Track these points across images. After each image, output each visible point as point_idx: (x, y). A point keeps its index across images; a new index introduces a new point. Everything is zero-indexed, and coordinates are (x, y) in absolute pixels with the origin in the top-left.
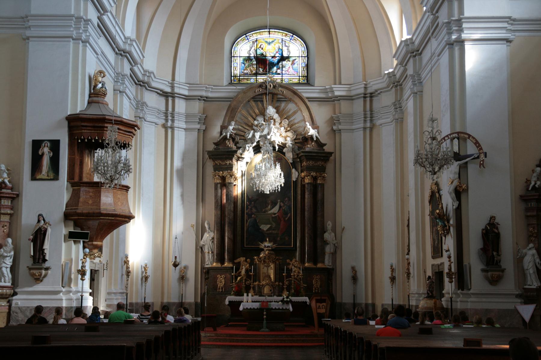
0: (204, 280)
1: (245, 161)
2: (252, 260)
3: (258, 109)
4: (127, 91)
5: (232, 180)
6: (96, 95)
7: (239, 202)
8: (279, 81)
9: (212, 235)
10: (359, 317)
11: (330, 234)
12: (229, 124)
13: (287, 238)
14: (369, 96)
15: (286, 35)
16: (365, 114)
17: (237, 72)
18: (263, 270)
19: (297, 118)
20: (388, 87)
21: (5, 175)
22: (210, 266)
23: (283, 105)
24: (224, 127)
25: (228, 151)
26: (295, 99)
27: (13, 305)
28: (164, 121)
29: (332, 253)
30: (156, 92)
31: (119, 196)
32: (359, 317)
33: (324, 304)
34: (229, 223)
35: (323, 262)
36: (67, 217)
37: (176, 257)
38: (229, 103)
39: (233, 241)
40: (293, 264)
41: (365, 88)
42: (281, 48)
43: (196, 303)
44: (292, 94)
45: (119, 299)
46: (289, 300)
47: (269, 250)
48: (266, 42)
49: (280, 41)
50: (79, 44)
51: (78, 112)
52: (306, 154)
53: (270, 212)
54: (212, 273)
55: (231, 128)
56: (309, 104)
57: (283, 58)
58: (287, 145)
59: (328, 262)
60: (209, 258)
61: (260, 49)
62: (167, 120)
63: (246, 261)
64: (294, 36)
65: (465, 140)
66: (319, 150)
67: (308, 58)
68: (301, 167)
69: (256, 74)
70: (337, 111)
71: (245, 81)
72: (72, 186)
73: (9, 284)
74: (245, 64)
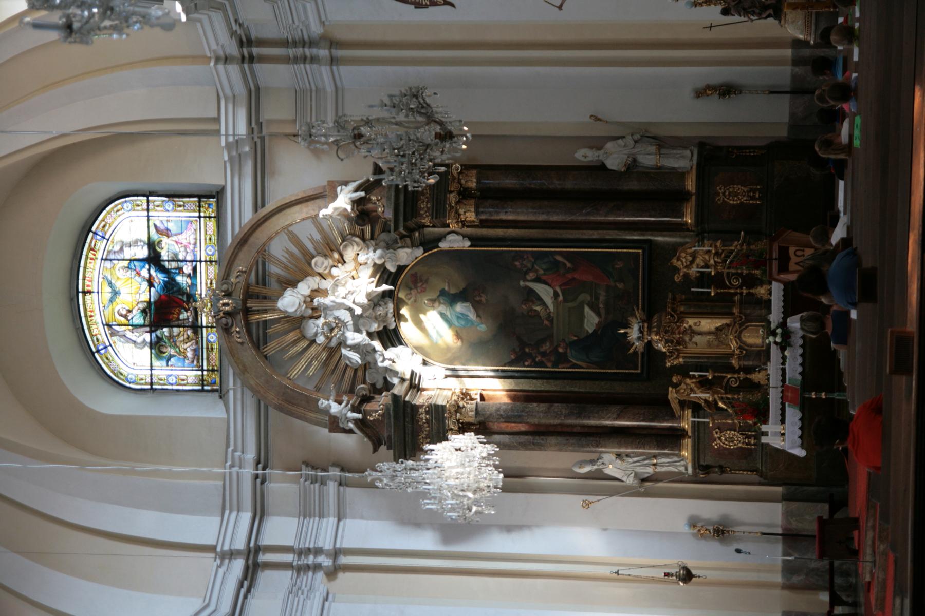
0: (725, 476)
1: (420, 369)
5: (471, 405)
7: (525, 385)
8: (213, 270)
10: (829, 330)
12: (326, 411)
13: (619, 265)
14: (249, 48)
15: (91, 249)
16: (295, 60)
17: (192, 375)
18: (700, 345)
23: (274, 269)
25: (396, 418)
28: (320, 575)
30: (245, 597)
32: (829, 330)
33: (792, 250)
34: (579, 415)
35: (681, 175)
38: (271, 409)
39: (625, 403)
40: (687, 267)
41: (227, 60)
42: (126, 263)
43: (786, 498)
44: (245, 248)
46: (779, 331)
47: (650, 328)
48: (111, 301)
49: (108, 264)
52: (401, 218)
54: (708, 460)
55: (335, 408)
56: (270, 207)
57: (154, 259)
58: (379, 262)
59: (683, 161)
61: (130, 316)
62: (317, 567)
63: (676, 386)
64: (93, 229)
69: (196, 328)
70: (289, 130)
71: (215, 355)
74: (171, 356)
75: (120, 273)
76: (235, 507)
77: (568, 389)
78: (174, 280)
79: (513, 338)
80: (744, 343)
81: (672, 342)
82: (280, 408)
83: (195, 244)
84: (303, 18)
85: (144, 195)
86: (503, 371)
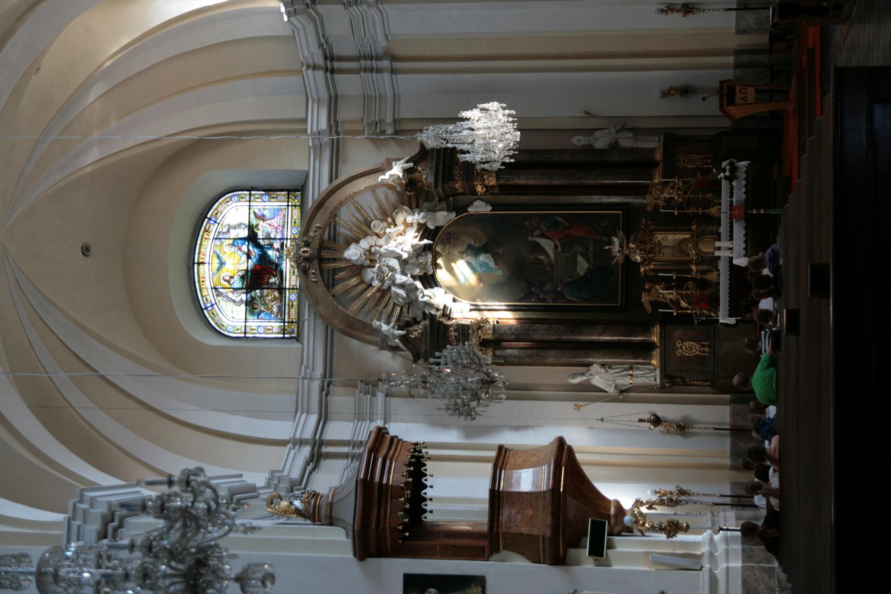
1: (450, 304)
6: (317, 513)
7: (530, 315)
9: (595, 368)
11: (597, 139)
12: (377, 331)
14: (331, 63)
15: (206, 231)
16: (365, 70)
17: (276, 325)
19: (370, 204)
20: (313, 20)
22: (658, 372)
23: (342, 230)
24: (384, 344)
25: (431, 333)
26: (333, 206)
29: (635, 135)
30: (311, 473)
33: (737, 89)
35: (652, 150)
36: (559, 560)
37: (641, 420)
38: (336, 333)
39: (607, 326)
41: (315, 68)
42: (231, 241)
43: (732, 402)
44: (322, 210)
48: (219, 270)
49: (218, 242)
51: (349, 542)
53: (552, 256)
55: (385, 328)
56: (341, 179)
57: (252, 238)
58: (422, 222)
59: (653, 143)
60: (642, 376)
63: (649, 291)
64: (209, 216)
66: (432, 157)
67: (253, 189)
68: (464, 194)
69: (281, 289)
70: (358, 127)
71: (294, 311)
72: (498, 551)
74: (261, 312)
75: (227, 249)
76: (305, 410)
77: (564, 317)
78: (266, 254)
79: (520, 278)
80: (700, 251)
81: (645, 251)
82: (343, 332)
83: (284, 226)
84: (372, 33)
85: (247, 190)
86: (514, 306)
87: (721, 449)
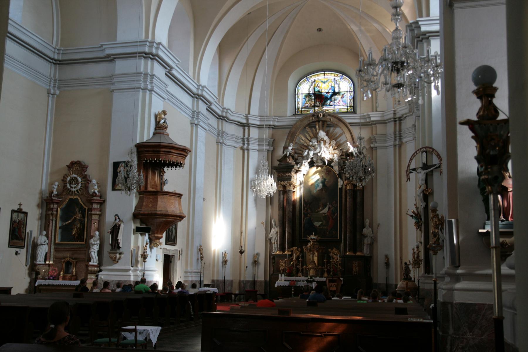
1: (302, 173)
2: (302, 249)
3: (313, 133)
4: (201, 123)
5: (291, 188)
12: (289, 146)
14: (398, 120)
15: (337, 75)
16: (395, 134)
17: (300, 105)
18: (310, 256)
21: (96, 187)
23: (332, 129)
27: (99, 278)
28: (241, 145)
31: (172, 201)
33: (336, 284)
35: (361, 251)
36: (135, 216)
38: (289, 130)
43: (265, 281)
45: (195, 278)
49: (333, 80)
50: (146, 92)
51: (145, 141)
53: (321, 212)
54: (276, 258)
55: (290, 148)
56: (350, 128)
57: (335, 94)
59: (366, 251)
62: (244, 144)
63: (297, 249)
65: (431, 153)
69: (314, 106)
70: (374, 132)
71: (306, 112)
72: (139, 194)
73: (96, 264)
75: (330, 84)
79: (312, 199)
82: (290, 132)
87: (247, 277)
